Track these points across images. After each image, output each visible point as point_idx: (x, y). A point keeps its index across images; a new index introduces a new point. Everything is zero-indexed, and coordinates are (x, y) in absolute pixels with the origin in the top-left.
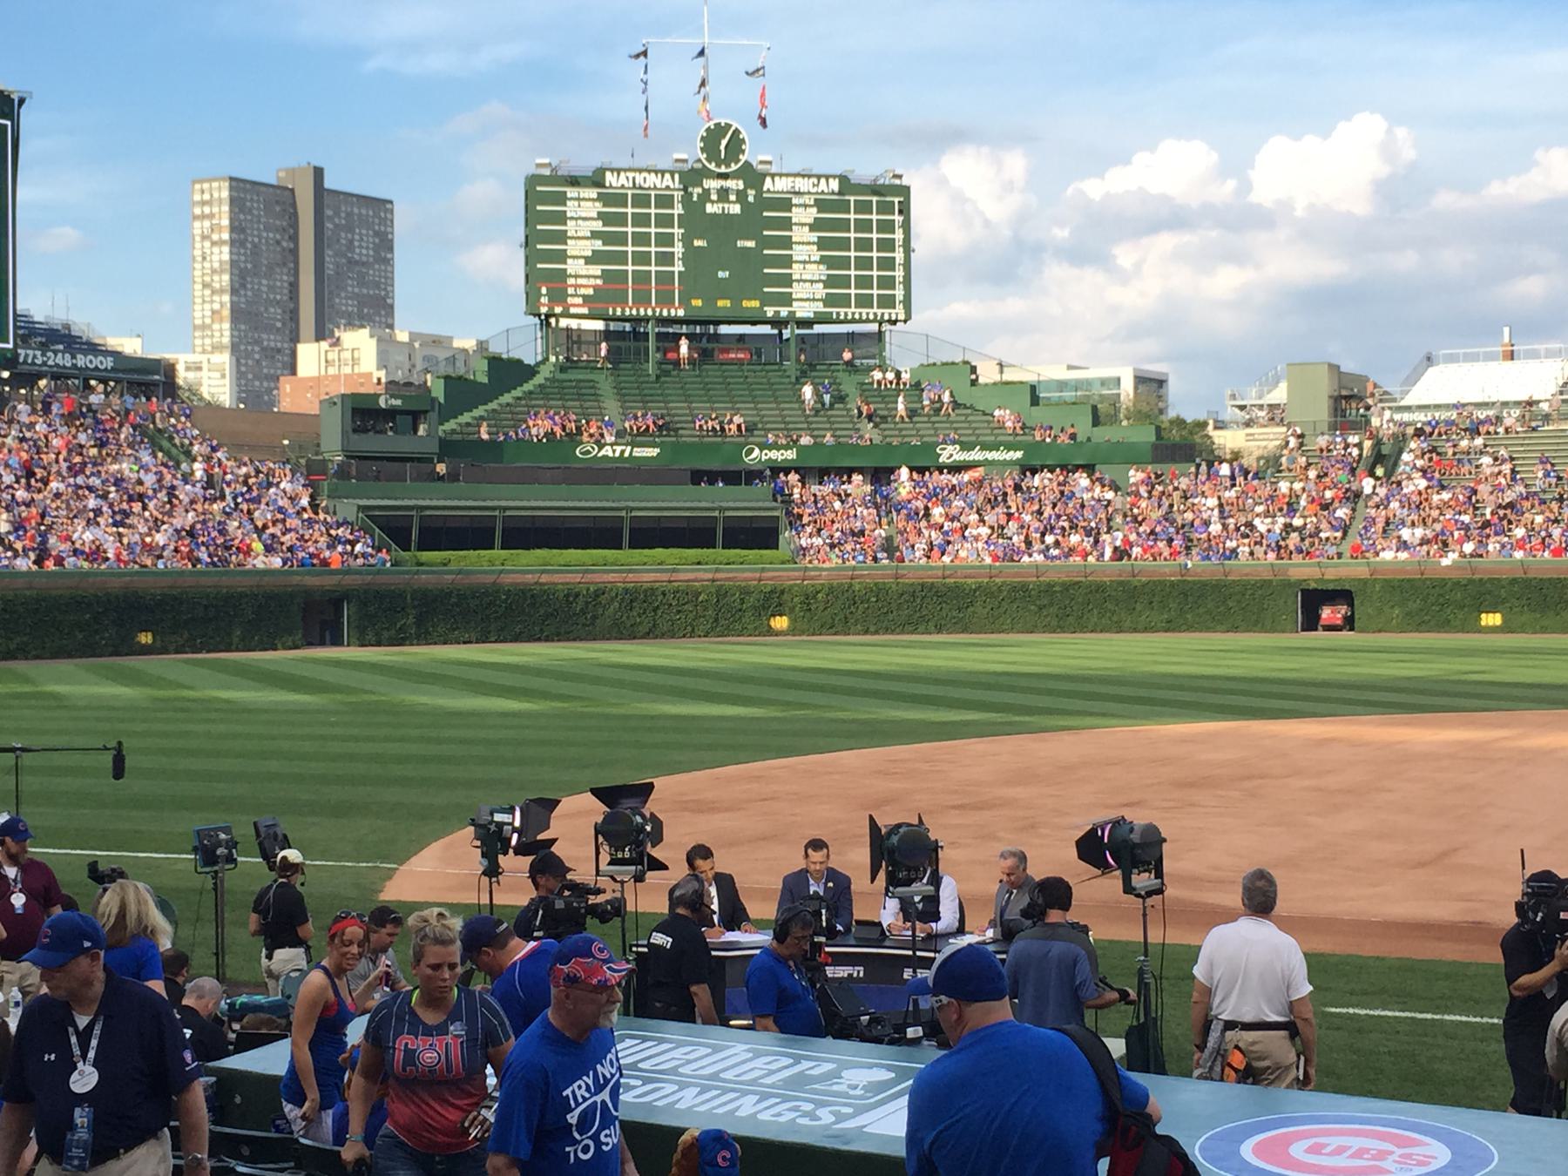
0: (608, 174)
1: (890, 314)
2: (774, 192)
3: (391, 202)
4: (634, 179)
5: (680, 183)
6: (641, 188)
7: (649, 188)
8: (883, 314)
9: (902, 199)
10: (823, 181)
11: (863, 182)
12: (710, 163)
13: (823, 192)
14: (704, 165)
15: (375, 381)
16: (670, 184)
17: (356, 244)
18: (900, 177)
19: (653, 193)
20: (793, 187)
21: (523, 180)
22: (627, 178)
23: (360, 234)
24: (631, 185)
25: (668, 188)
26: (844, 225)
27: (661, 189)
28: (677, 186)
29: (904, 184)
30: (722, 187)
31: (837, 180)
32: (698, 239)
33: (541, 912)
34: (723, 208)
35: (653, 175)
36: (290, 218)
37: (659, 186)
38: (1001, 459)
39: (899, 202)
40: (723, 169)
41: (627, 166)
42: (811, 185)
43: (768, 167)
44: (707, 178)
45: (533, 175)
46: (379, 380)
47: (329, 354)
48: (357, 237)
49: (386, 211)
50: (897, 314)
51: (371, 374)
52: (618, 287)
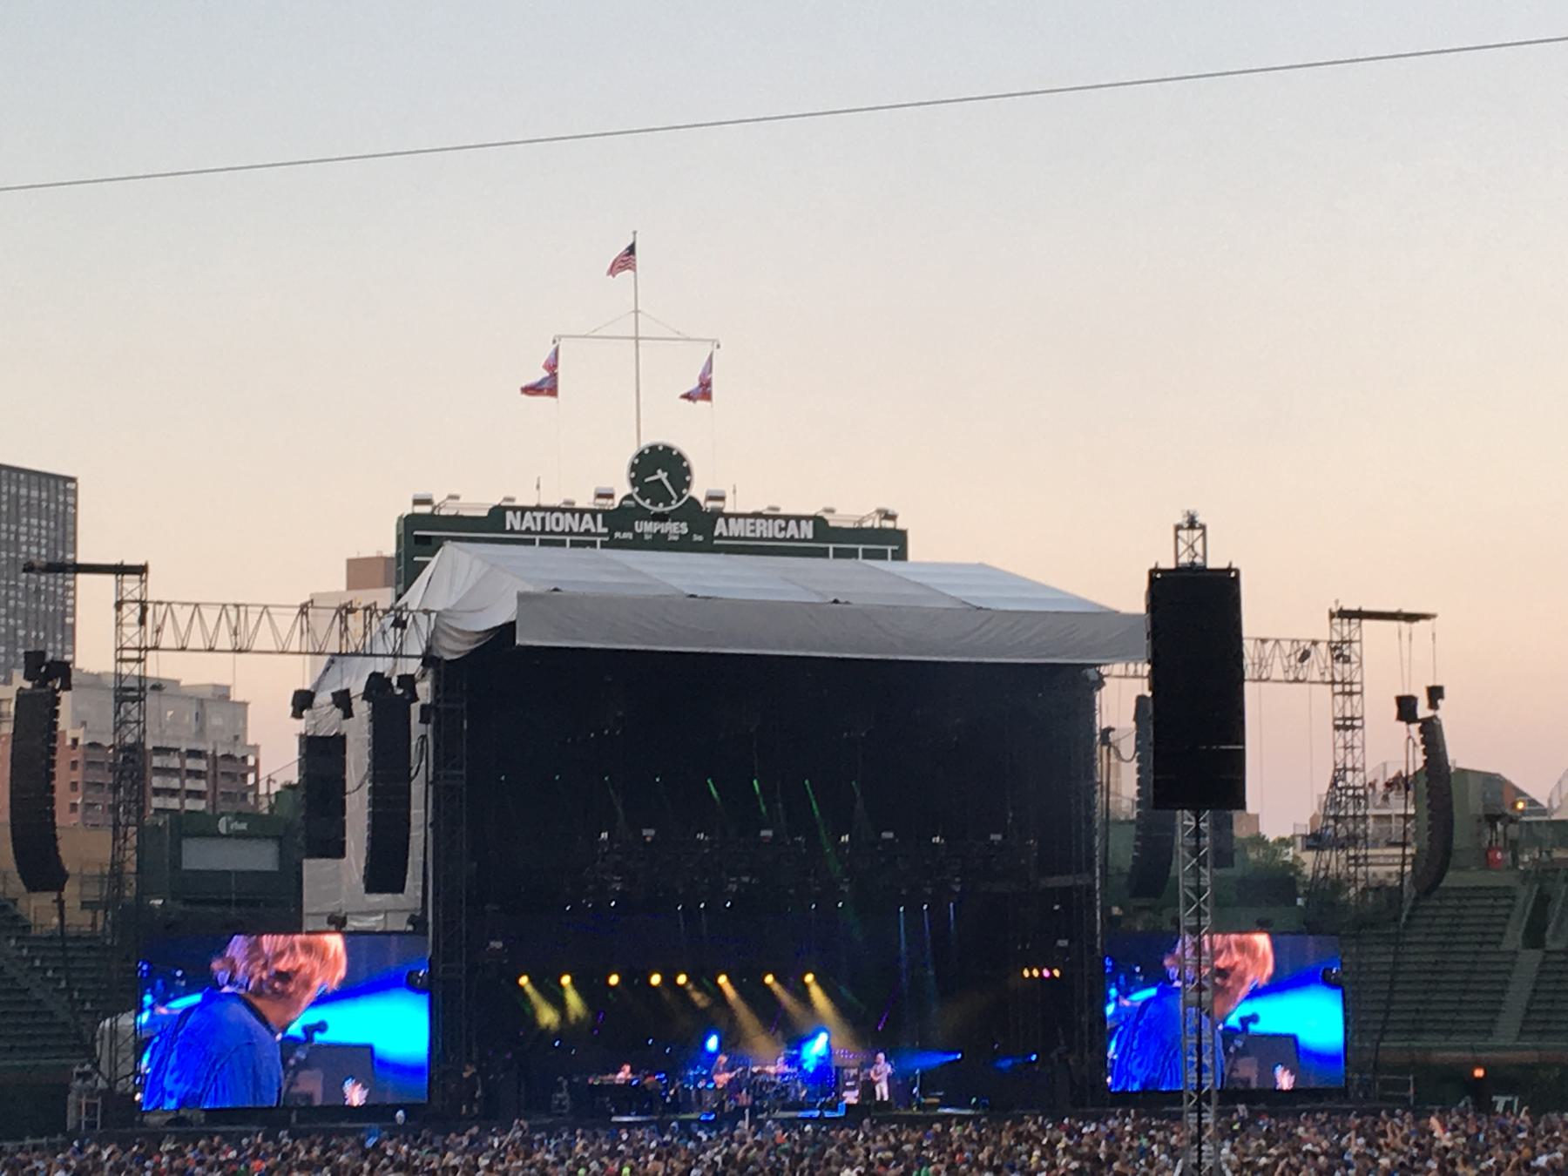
0: (509, 514)
2: (728, 538)
3: (73, 480)
4: (543, 519)
5: (604, 525)
6: (552, 532)
7: (563, 533)
9: (896, 548)
10: (792, 523)
12: (644, 500)
13: (792, 539)
14: (637, 503)
15: (69, 742)
16: (591, 526)
17: (23, 538)
20: (753, 531)
21: (395, 521)
22: (535, 519)
23: (28, 525)
24: (539, 529)
25: (587, 532)
27: (578, 534)
28: (601, 529)
30: (659, 531)
31: (811, 522)
33: (1167, 1109)
35: (568, 515)
37: (575, 529)
39: (893, 551)
40: (661, 508)
41: (533, 504)
42: (777, 529)
43: (718, 504)
46: (75, 741)
48: (23, 529)
49: (66, 491)
52: (1175, 1109)
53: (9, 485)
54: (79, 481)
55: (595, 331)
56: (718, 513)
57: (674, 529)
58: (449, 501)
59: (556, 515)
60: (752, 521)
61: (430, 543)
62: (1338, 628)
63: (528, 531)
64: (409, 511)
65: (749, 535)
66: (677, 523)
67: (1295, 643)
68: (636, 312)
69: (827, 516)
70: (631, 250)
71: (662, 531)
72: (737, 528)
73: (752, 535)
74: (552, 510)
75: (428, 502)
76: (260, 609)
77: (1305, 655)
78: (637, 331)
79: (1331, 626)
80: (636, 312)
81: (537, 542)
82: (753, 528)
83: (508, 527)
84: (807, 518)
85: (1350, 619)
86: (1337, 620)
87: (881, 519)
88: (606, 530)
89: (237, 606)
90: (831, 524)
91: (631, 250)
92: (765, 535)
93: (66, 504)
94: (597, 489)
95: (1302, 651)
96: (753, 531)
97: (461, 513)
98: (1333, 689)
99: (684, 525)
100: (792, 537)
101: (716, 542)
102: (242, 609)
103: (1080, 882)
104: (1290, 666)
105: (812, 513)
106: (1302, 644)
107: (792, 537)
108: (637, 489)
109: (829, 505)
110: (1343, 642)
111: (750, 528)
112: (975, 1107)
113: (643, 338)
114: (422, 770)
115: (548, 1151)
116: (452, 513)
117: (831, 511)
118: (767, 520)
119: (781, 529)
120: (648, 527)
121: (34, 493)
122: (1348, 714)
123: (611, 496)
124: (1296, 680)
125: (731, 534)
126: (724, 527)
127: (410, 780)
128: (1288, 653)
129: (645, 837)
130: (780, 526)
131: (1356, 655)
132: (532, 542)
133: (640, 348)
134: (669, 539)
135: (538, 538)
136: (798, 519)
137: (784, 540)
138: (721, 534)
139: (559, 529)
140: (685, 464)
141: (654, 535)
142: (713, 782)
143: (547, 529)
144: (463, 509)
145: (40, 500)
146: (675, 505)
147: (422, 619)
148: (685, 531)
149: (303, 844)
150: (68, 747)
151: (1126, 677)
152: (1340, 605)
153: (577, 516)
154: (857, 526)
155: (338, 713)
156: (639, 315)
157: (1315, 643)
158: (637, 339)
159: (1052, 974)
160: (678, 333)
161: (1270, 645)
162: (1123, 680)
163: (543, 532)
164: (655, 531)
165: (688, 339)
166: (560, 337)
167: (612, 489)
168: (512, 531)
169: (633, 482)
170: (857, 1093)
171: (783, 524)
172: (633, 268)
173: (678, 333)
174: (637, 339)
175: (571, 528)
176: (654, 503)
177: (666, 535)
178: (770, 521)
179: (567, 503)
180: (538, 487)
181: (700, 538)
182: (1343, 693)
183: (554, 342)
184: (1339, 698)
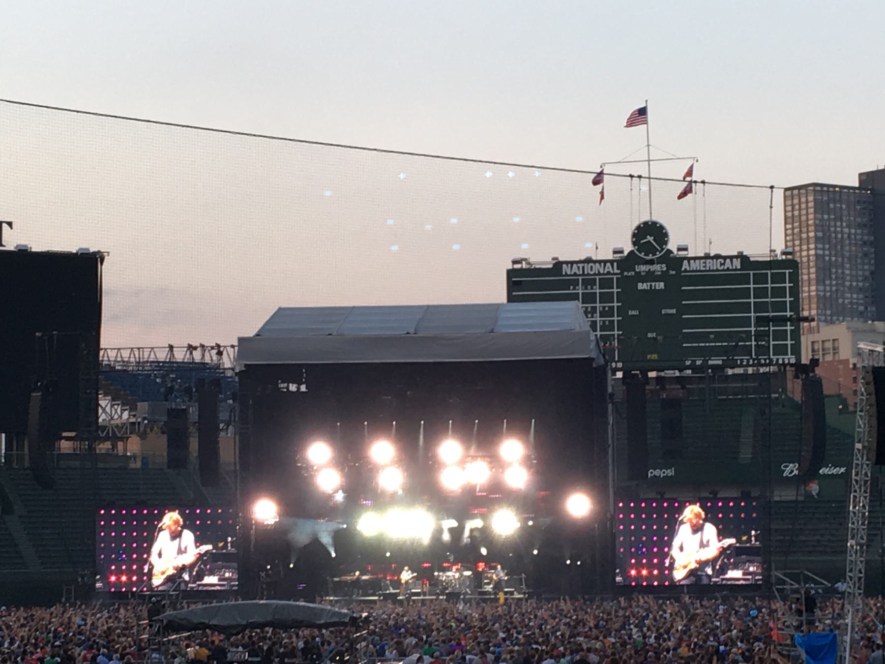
0: (564, 266)
1: (783, 359)
4: (583, 268)
5: (618, 269)
6: (588, 274)
7: (595, 274)
8: (778, 360)
9: (791, 271)
10: (728, 261)
12: (641, 253)
13: (728, 269)
15: (851, 366)
19: (597, 277)
22: (578, 268)
24: (581, 273)
25: (609, 273)
26: (746, 293)
27: (603, 274)
28: (616, 271)
30: (649, 270)
31: (739, 260)
32: (632, 310)
34: (651, 285)
35: (597, 264)
36: (870, 215)
37: (602, 272)
38: (830, 473)
39: (789, 273)
40: (650, 257)
42: (719, 264)
43: (685, 253)
44: (639, 264)
46: (855, 365)
50: (789, 359)
51: (847, 361)
55: (624, 159)
59: (590, 264)
60: (704, 261)
61: (521, 284)
64: (510, 267)
68: (648, 145)
70: (642, 112)
71: (651, 270)
73: (704, 269)
76: (149, 350)
78: (649, 157)
80: (648, 145)
82: (704, 265)
83: (564, 273)
88: (619, 271)
89: (139, 349)
91: (642, 112)
94: (614, 249)
100: (728, 268)
101: (683, 274)
102: (141, 350)
108: (636, 247)
111: (702, 265)
113: (652, 160)
115: (534, 634)
119: (721, 264)
120: (643, 268)
123: (622, 252)
126: (730, 264)
130: (720, 262)
134: (656, 274)
137: (723, 270)
138: (685, 269)
139: (592, 273)
140: (664, 231)
141: (647, 272)
142: (535, 421)
143: (586, 273)
146: (658, 255)
147: (230, 350)
148: (665, 269)
150: (850, 369)
156: (650, 147)
158: (649, 161)
163: (583, 274)
164: (647, 270)
165: (679, 159)
166: (604, 164)
167: (687, 245)
168: (566, 275)
169: (634, 244)
171: (723, 261)
172: (645, 122)
174: (649, 161)
175: (599, 271)
176: (647, 255)
177: (654, 272)
178: (715, 260)
181: (674, 273)
183: (601, 167)
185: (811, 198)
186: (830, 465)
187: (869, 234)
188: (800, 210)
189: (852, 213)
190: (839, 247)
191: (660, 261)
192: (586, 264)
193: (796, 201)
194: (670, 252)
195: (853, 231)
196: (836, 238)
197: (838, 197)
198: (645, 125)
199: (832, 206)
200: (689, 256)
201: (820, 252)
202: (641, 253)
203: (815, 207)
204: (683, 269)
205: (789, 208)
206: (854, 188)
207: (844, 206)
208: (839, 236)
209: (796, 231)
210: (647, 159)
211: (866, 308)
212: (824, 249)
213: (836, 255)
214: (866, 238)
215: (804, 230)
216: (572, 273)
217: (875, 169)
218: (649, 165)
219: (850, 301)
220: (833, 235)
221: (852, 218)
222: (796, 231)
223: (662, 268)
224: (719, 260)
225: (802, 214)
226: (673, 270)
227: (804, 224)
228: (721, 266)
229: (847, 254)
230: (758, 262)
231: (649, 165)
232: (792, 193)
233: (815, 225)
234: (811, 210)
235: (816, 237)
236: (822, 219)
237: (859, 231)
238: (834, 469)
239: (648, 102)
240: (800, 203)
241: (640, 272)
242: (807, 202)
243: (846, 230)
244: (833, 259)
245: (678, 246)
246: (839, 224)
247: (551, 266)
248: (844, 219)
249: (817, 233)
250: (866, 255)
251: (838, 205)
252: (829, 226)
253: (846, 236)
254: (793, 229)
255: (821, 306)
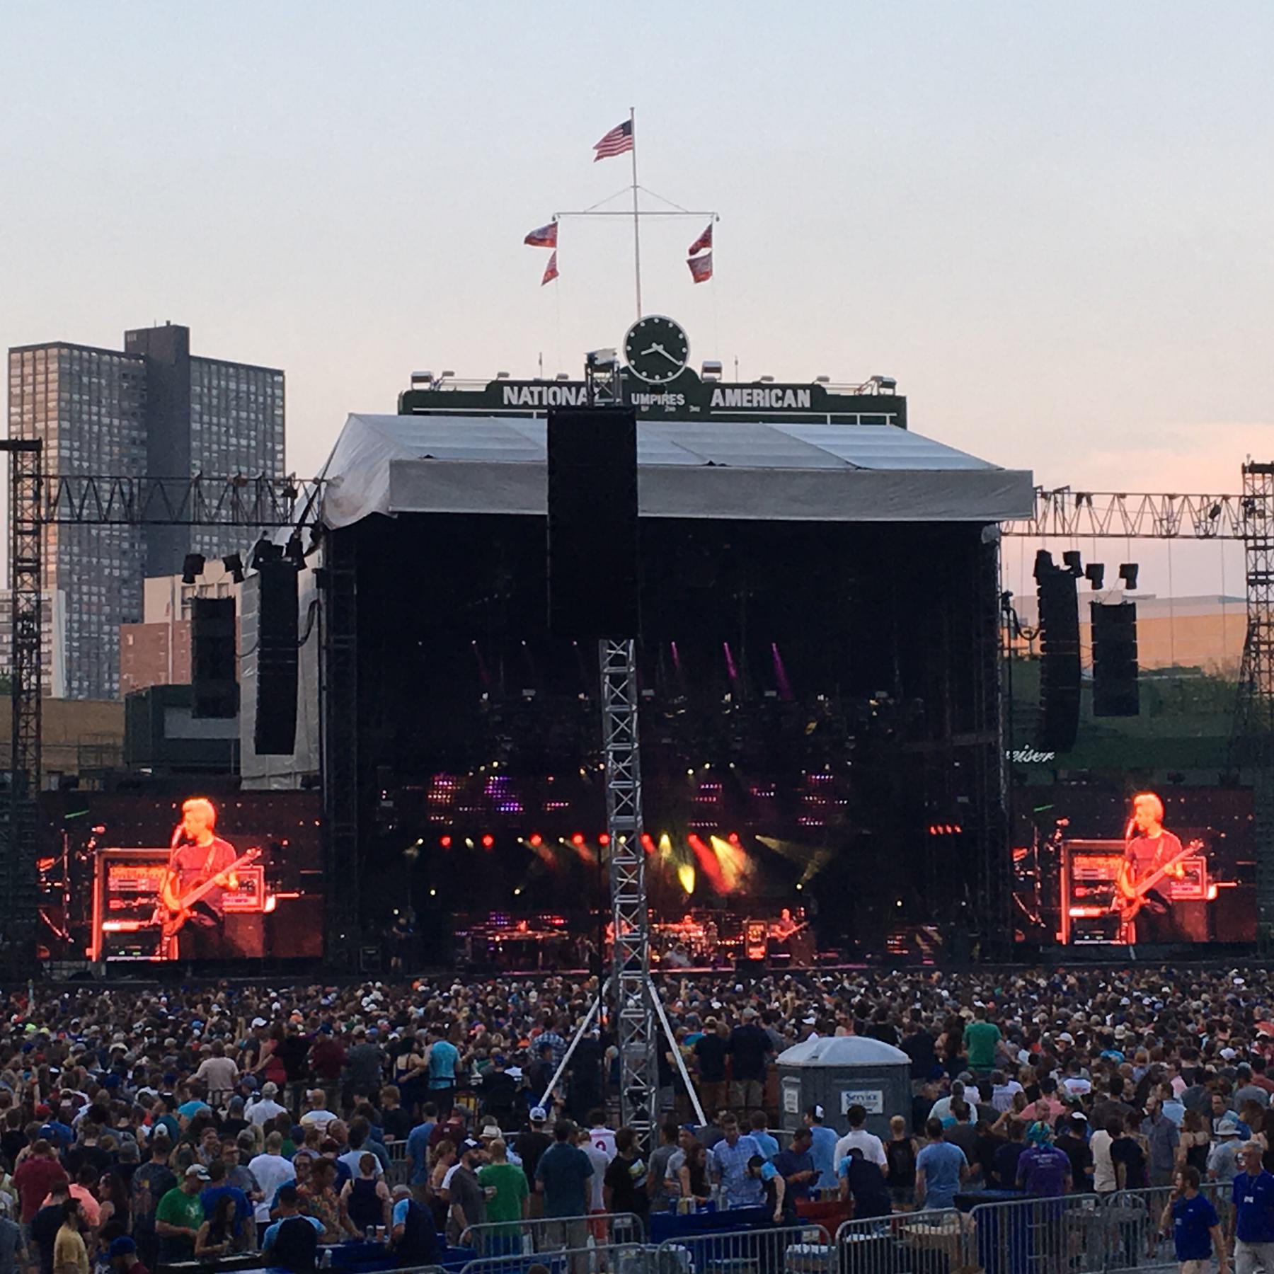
0: (507, 389)
3: (280, 373)
4: (540, 394)
9: (895, 414)
10: (789, 392)
11: (843, 393)
13: (790, 408)
18: (891, 385)
21: (397, 398)
22: (532, 393)
24: (536, 403)
29: (897, 394)
30: (656, 403)
31: (808, 391)
35: (565, 389)
40: (657, 380)
43: (716, 375)
45: (408, 393)
47: (187, 591)
49: (274, 383)
53: (219, 380)
54: (286, 374)
56: (714, 385)
57: (667, 399)
58: (445, 378)
60: (749, 391)
62: (1250, 482)
63: (526, 405)
65: (746, 404)
66: (672, 395)
67: (1205, 499)
69: (824, 385)
70: (627, 128)
72: (733, 398)
74: (549, 384)
75: (426, 379)
77: (1216, 511)
79: (1245, 482)
81: (535, 415)
82: (750, 398)
83: (506, 402)
84: (804, 387)
85: (1263, 474)
86: (1248, 475)
87: (880, 386)
90: (829, 392)
91: (627, 128)
92: (762, 405)
93: (273, 396)
95: (1212, 506)
96: (749, 401)
97: (459, 389)
98: (1246, 544)
99: (680, 396)
100: (526, 403)
101: (713, 413)
103: (981, 741)
104: (1200, 521)
105: (810, 382)
106: (1212, 499)
107: (526, 403)
109: (823, 374)
110: (1255, 496)
112: (868, 962)
114: (315, 629)
116: (451, 389)
117: (826, 379)
118: (560, 388)
119: (778, 398)
121: (244, 387)
122: (1261, 568)
124: (1207, 536)
125: (727, 405)
126: (721, 397)
127: (297, 644)
128: (1197, 508)
129: (526, 697)
130: (777, 395)
131: (1190, 505)
132: (530, 416)
133: (639, 223)
135: (535, 412)
136: (795, 388)
137: (781, 409)
141: (650, 406)
144: (461, 385)
145: (248, 392)
146: (671, 377)
148: (682, 402)
149: (10, 681)
151: (1029, 535)
152: (1251, 459)
153: (574, 389)
154: (857, 393)
155: (229, 576)
157: (1226, 498)
158: (636, 214)
159: (954, 830)
160: (678, 207)
161: (1177, 503)
162: (1026, 538)
165: (688, 213)
166: (559, 214)
168: (510, 405)
170: (763, 949)
172: (630, 146)
173: (678, 207)
174: (636, 214)
178: (767, 391)
179: (559, 377)
180: (540, 362)
181: (697, 409)
182: (1256, 548)
184: (1252, 553)
185: (54, 366)
186: (1027, 747)
187: (139, 429)
188: (34, 384)
189: (116, 393)
190: (95, 447)
191: (672, 388)
192: (545, 388)
193: (28, 370)
194: (689, 372)
195: (116, 422)
196: (90, 431)
197: (94, 367)
198: (631, 151)
199: (85, 380)
200: (723, 381)
201: (66, 453)
202: (640, 373)
203: (60, 381)
204: (713, 404)
205: (16, 381)
206: (118, 354)
207: (103, 381)
208: (96, 428)
209: (27, 417)
210: (633, 211)
211: (132, 545)
212: (71, 449)
213: (89, 460)
214: (134, 433)
215: (41, 416)
216: (521, 402)
217: (151, 326)
218: (636, 221)
219: (108, 532)
220: (86, 427)
221: (115, 402)
222: (27, 417)
223: (677, 400)
224: (774, 391)
225: (37, 390)
226: (695, 406)
227: (40, 407)
228: (777, 401)
229: (107, 458)
230: (838, 396)
231: (636, 221)
232: (22, 356)
233: (60, 410)
234: (54, 386)
235: (61, 430)
236: (71, 401)
237: (125, 423)
238: (1033, 754)
239: (635, 111)
240: (35, 374)
241: (639, 406)
242: (47, 372)
243: (106, 420)
244: (85, 465)
245: (705, 363)
246: (94, 409)
247: (483, 389)
248: (104, 401)
249: (62, 422)
250: (134, 460)
251: (95, 380)
252: (81, 412)
253: (105, 429)
254: (22, 414)
255: (65, 539)
